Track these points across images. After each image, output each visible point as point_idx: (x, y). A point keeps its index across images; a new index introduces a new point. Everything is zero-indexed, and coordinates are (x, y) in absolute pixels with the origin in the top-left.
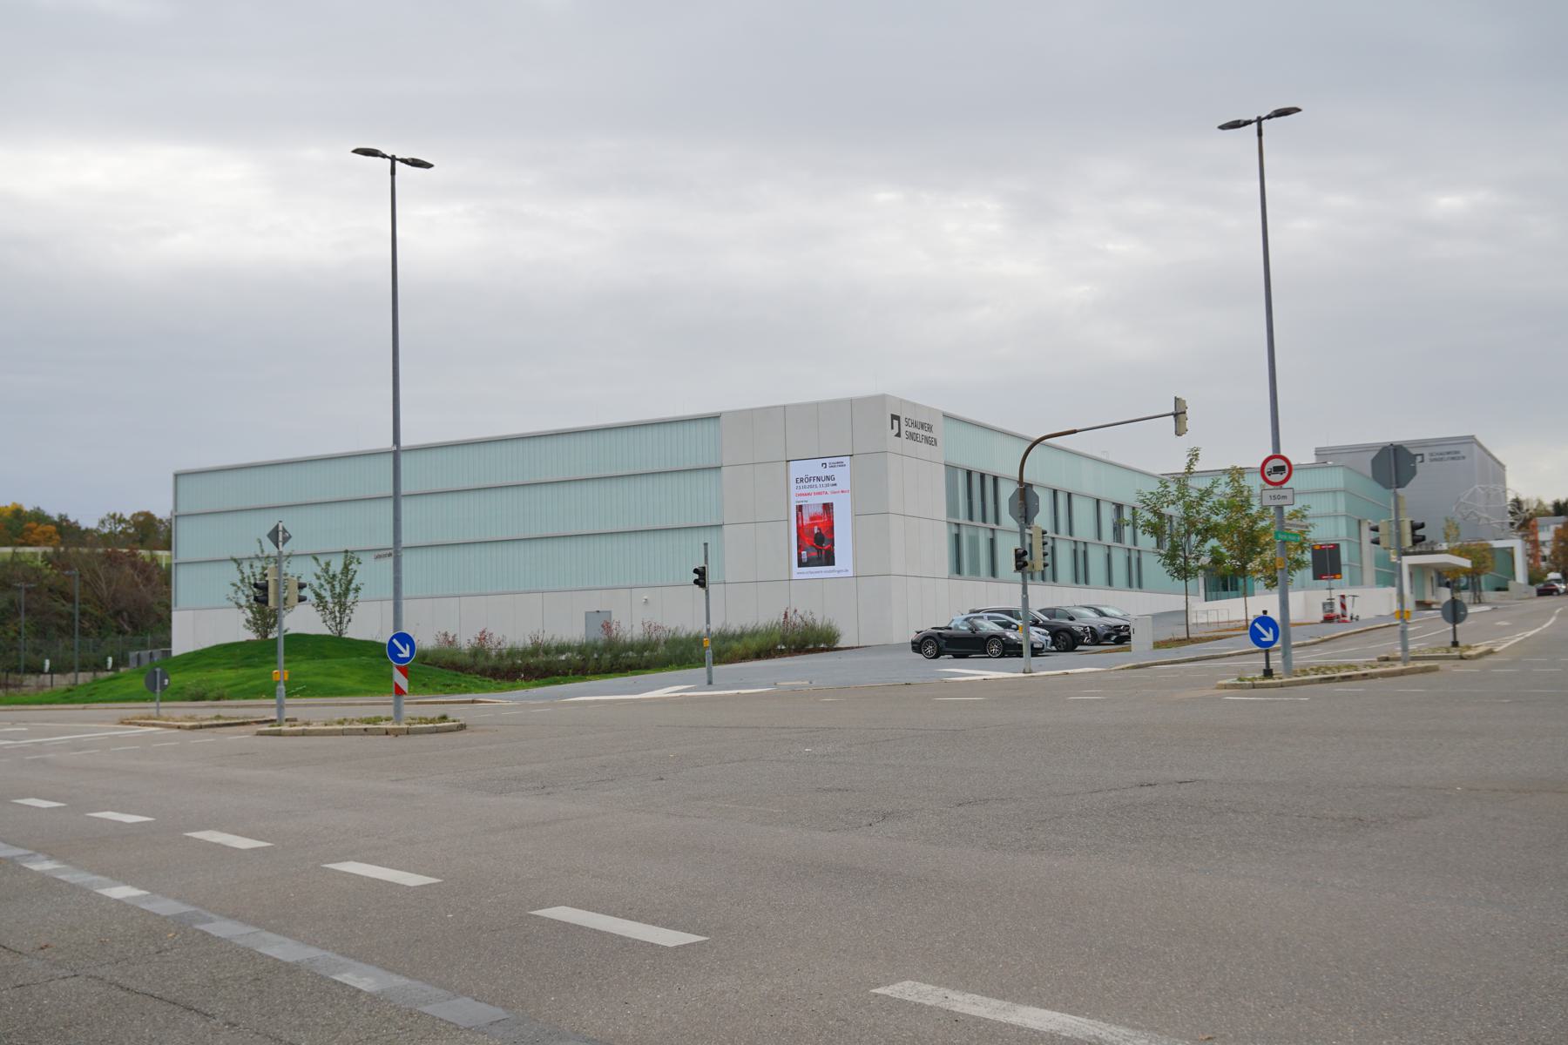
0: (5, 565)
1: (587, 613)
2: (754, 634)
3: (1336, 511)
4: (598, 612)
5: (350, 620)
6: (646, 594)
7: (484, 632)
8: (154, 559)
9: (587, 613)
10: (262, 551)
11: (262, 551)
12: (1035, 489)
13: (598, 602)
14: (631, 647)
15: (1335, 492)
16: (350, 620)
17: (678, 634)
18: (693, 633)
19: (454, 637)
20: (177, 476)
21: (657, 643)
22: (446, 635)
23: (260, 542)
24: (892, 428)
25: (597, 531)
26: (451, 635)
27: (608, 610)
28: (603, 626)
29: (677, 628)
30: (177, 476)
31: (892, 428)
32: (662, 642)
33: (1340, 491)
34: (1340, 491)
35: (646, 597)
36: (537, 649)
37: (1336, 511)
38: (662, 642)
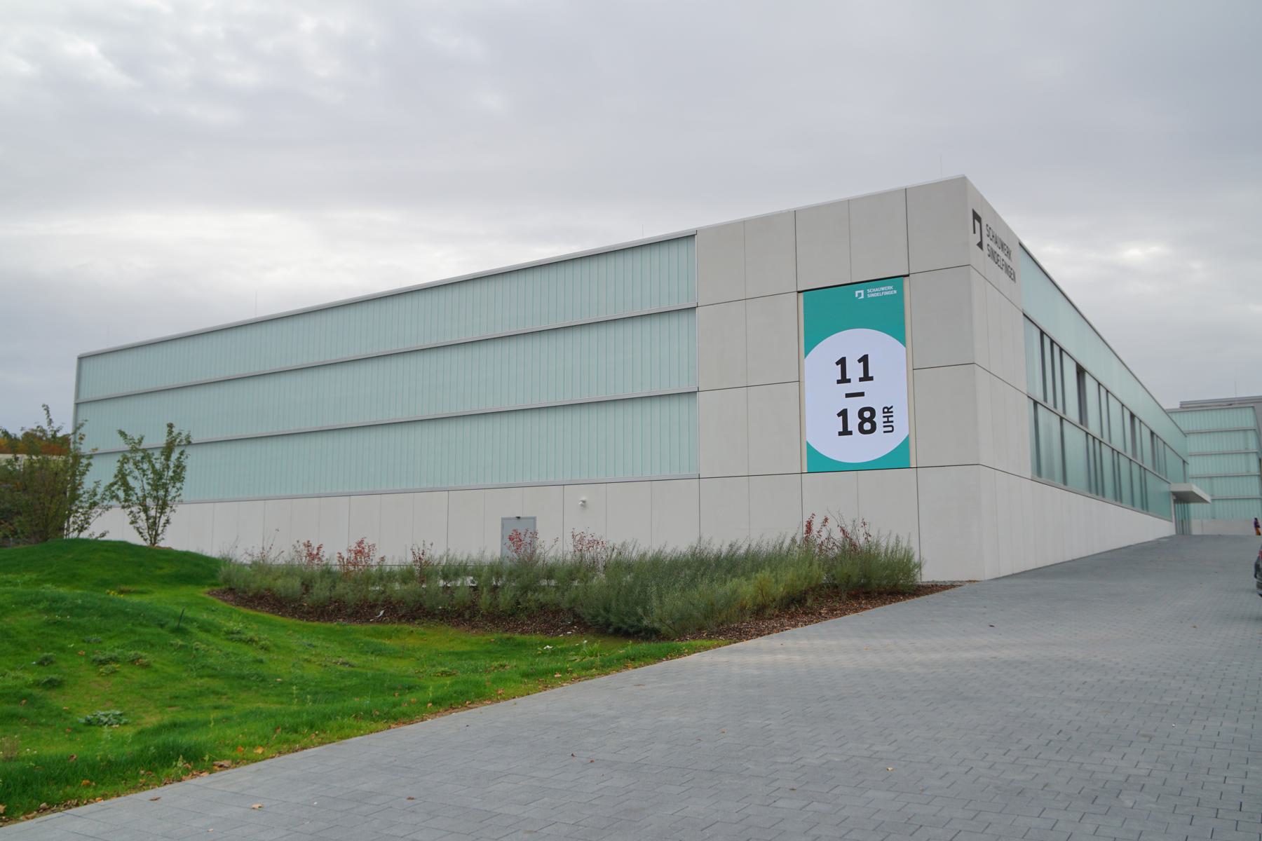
0: (5, 476)
1: (503, 519)
2: (453, 571)
3: (1246, 449)
4: (519, 518)
5: (168, 521)
6: (583, 494)
7: (361, 542)
8: (37, 457)
9: (503, 519)
10: (50, 421)
11: (50, 421)
12: (1087, 375)
13: (517, 504)
14: (550, 573)
15: (1245, 430)
16: (168, 521)
17: (626, 554)
18: (650, 554)
19: (319, 548)
20: (81, 359)
21: (592, 567)
22: (308, 545)
23: (47, 409)
24: (974, 232)
25: (536, 404)
26: (315, 545)
27: (75, 361)
28: (511, 539)
29: (623, 545)
30: (81, 359)
31: (974, 232)
32: (600, 567)
33: (1251, 430)
34: (1251, 430)
35: (584, 499)
36: (423, 571)
37: (1246, 449)
38: (600, 567)
